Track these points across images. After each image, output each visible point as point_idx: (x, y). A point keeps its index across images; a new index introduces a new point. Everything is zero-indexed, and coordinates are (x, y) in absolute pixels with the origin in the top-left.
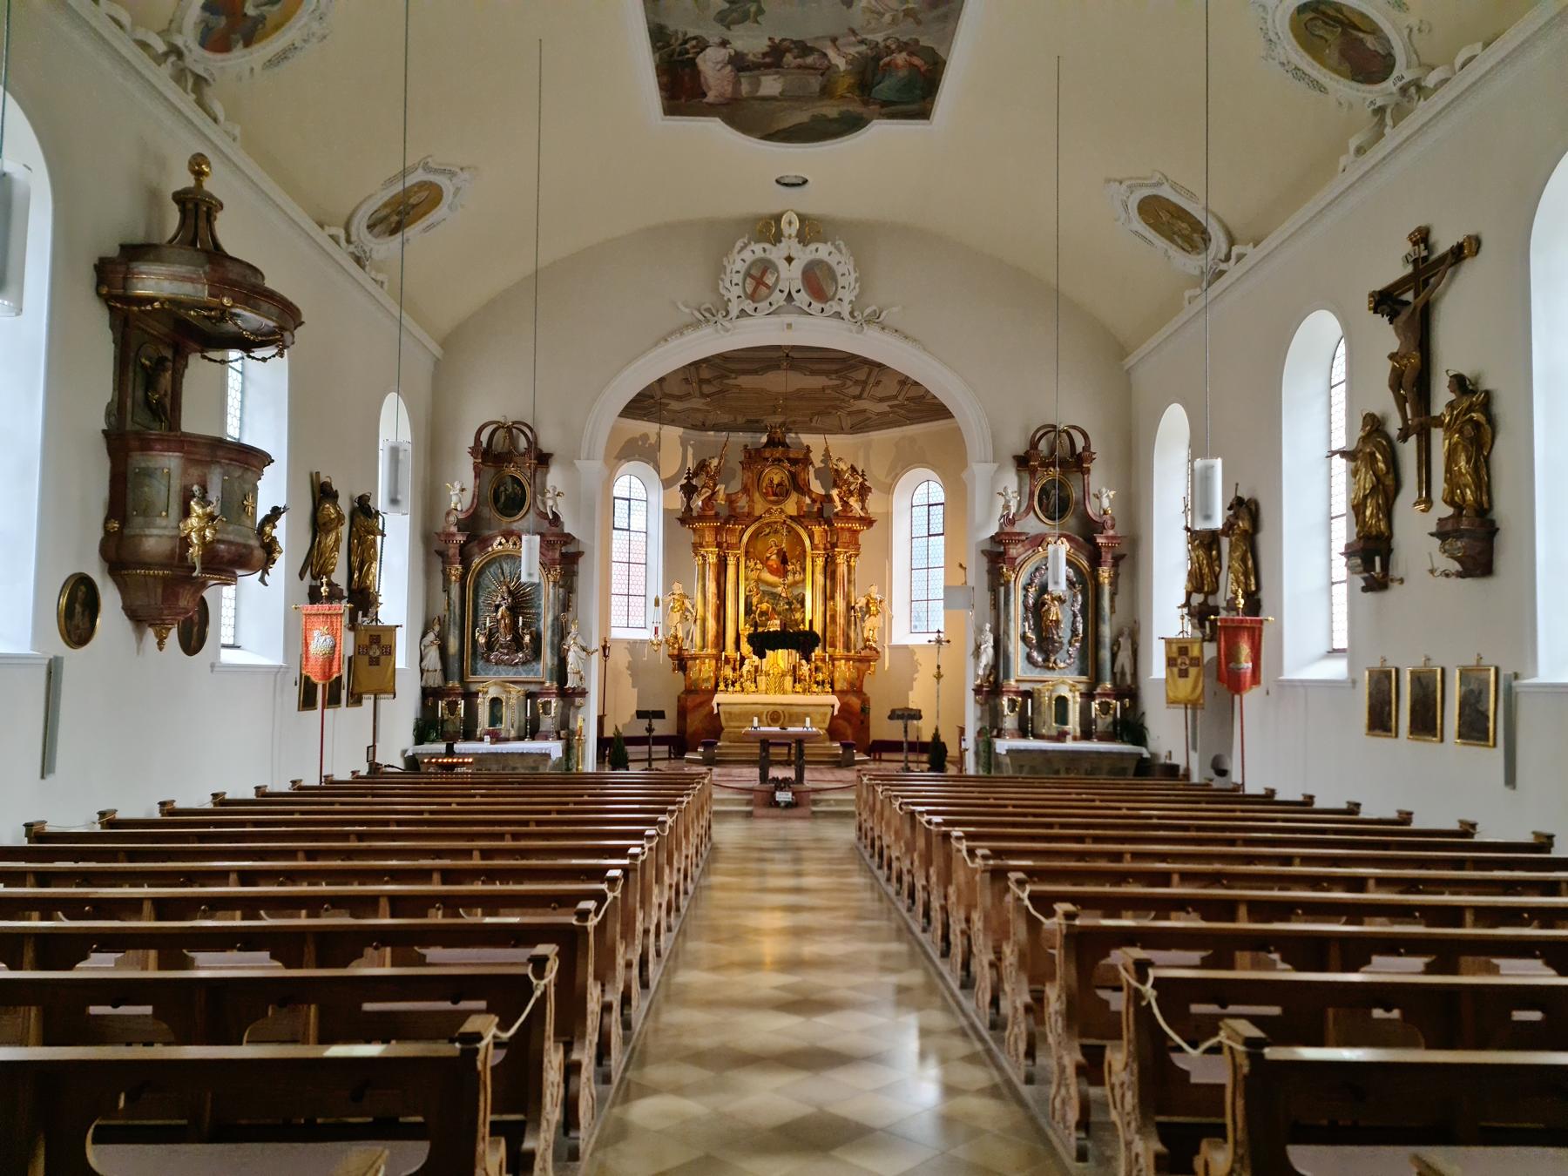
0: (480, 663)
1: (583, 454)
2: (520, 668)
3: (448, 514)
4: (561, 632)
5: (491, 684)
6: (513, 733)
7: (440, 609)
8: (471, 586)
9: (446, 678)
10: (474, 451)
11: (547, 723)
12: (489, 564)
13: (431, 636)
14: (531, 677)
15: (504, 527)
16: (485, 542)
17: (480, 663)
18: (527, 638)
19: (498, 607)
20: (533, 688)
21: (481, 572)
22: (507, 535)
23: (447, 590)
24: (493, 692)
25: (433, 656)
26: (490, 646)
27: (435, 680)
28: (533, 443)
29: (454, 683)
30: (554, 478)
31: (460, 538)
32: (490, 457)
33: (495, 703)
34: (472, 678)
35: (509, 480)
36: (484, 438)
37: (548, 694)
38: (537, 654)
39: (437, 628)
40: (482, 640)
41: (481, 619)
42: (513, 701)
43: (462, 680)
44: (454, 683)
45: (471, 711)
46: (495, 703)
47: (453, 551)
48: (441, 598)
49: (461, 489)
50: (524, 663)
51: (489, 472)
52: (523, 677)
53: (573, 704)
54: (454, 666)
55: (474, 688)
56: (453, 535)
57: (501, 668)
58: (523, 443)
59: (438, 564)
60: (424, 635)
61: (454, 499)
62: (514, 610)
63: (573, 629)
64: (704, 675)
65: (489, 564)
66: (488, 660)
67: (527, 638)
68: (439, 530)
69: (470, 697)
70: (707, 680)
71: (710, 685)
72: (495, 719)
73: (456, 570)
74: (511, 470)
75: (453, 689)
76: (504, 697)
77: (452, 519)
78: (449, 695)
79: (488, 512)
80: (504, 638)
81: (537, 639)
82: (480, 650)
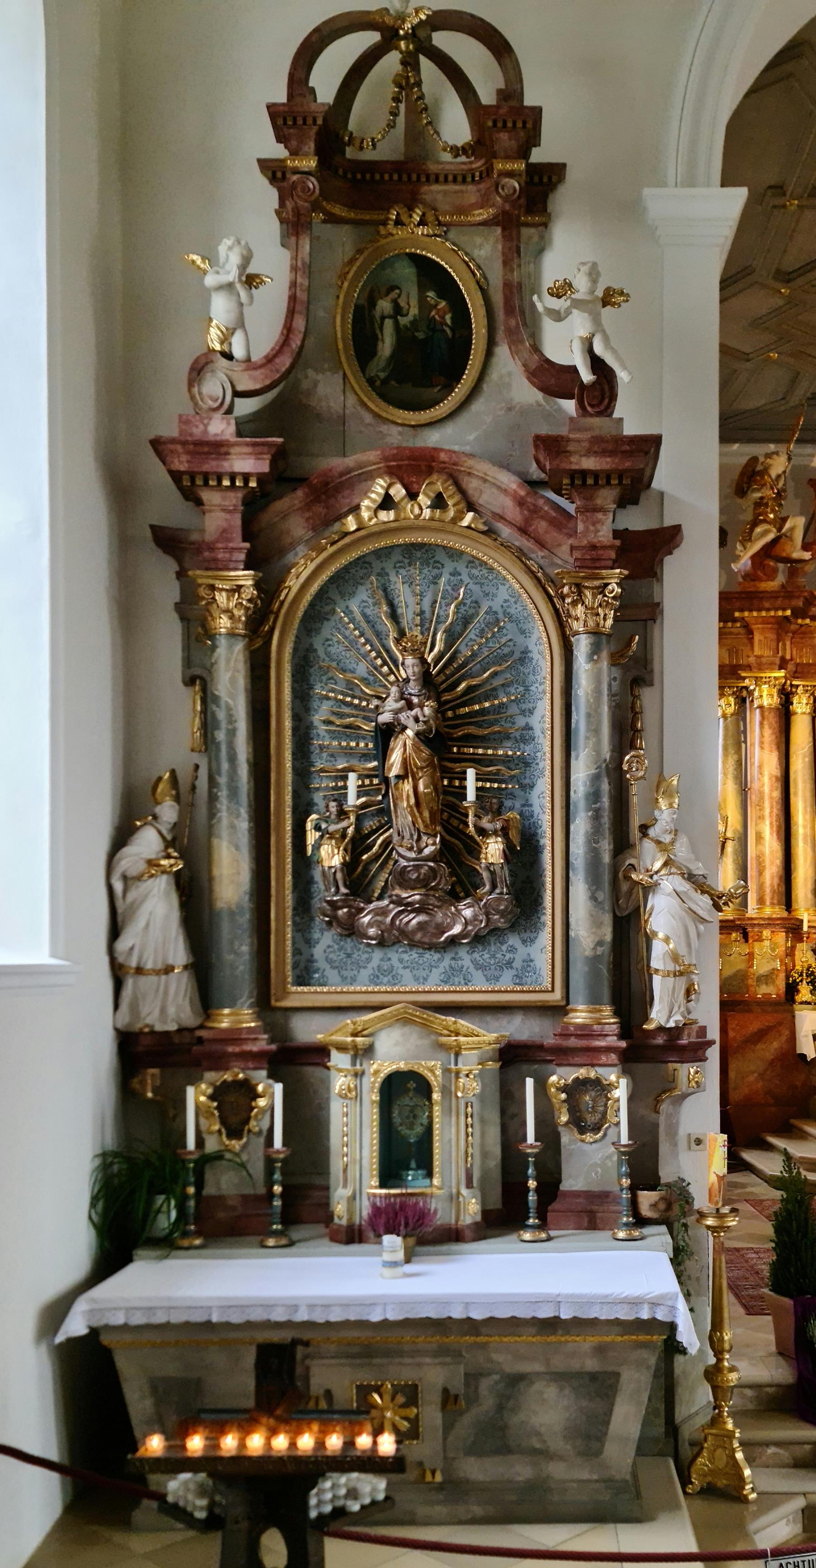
0: (325, 942)
1: (673, 168)
2: (465, 957)
3: (199, 369)
4: (621, 829)
5: (384, 1024)
6: (472, 1209)
7: (175, 743)
8: (283, 644)
9: (207, 997)
10: (286, 120)
11: (592, 1162)
12: (342, 582)
13: (148, 842)
14: (505, 989)
15: (395, 437)
16: (329, 497)
17: (325, 942)
18: (493, 850)
19: (386, 734)
20: (521, 1029)
21: (317, 614)
22: (413, 468)
23: (198, 678)
24: (394, 1050)
25: (157, 912)
26: (357, 879)
27: (168, 1005)
28: (509, 122)
29: (236, 1017)
30: (567, 253)
31: (246, 463)
32: (336, 174)
33: (403, 1091)
34: (299, 996)
35: (406, 273)
36: (326, 79)
37: (591, 1055)
38: (524, 900)
39: (168, 812)
40: (332, 857)
41: (322, 784)
42: (470, 1087)
43: (264, 1002)
44: (236, 1017)
45: (307, 1120)
46: (403, 1091)
47: (220, 515)
48: (179, 711)
49: (241, 282)
50: (478, 940)
51: (341, 241)
52: (479, 988)
53: (668, 1085)
54: (236, 954)
55: (308, 1030)
56: (218, 448)
57: (397, 956)
58: (455, 126)
59: (162, 582)
60: (122, 837)
61: (221, 309)
62: (444, 746)
63: (665, 814)
64: (761, 967)
65: (342, 582)
66: (351, 930)
67: (493, 850)
68: (169, 430)
69: (295, 1062)
70: (768, 978)
71: (775, 990)
72: (403, 1152)
73: (233, 590)
74: (414, 234)
75: (234, 1036)
76: (432, 1068)
77: (214, 387)
78: (219, 1062)
79: (333, 391)
80: (411, 840)
81: (524, 852)
82: (324, 894)
